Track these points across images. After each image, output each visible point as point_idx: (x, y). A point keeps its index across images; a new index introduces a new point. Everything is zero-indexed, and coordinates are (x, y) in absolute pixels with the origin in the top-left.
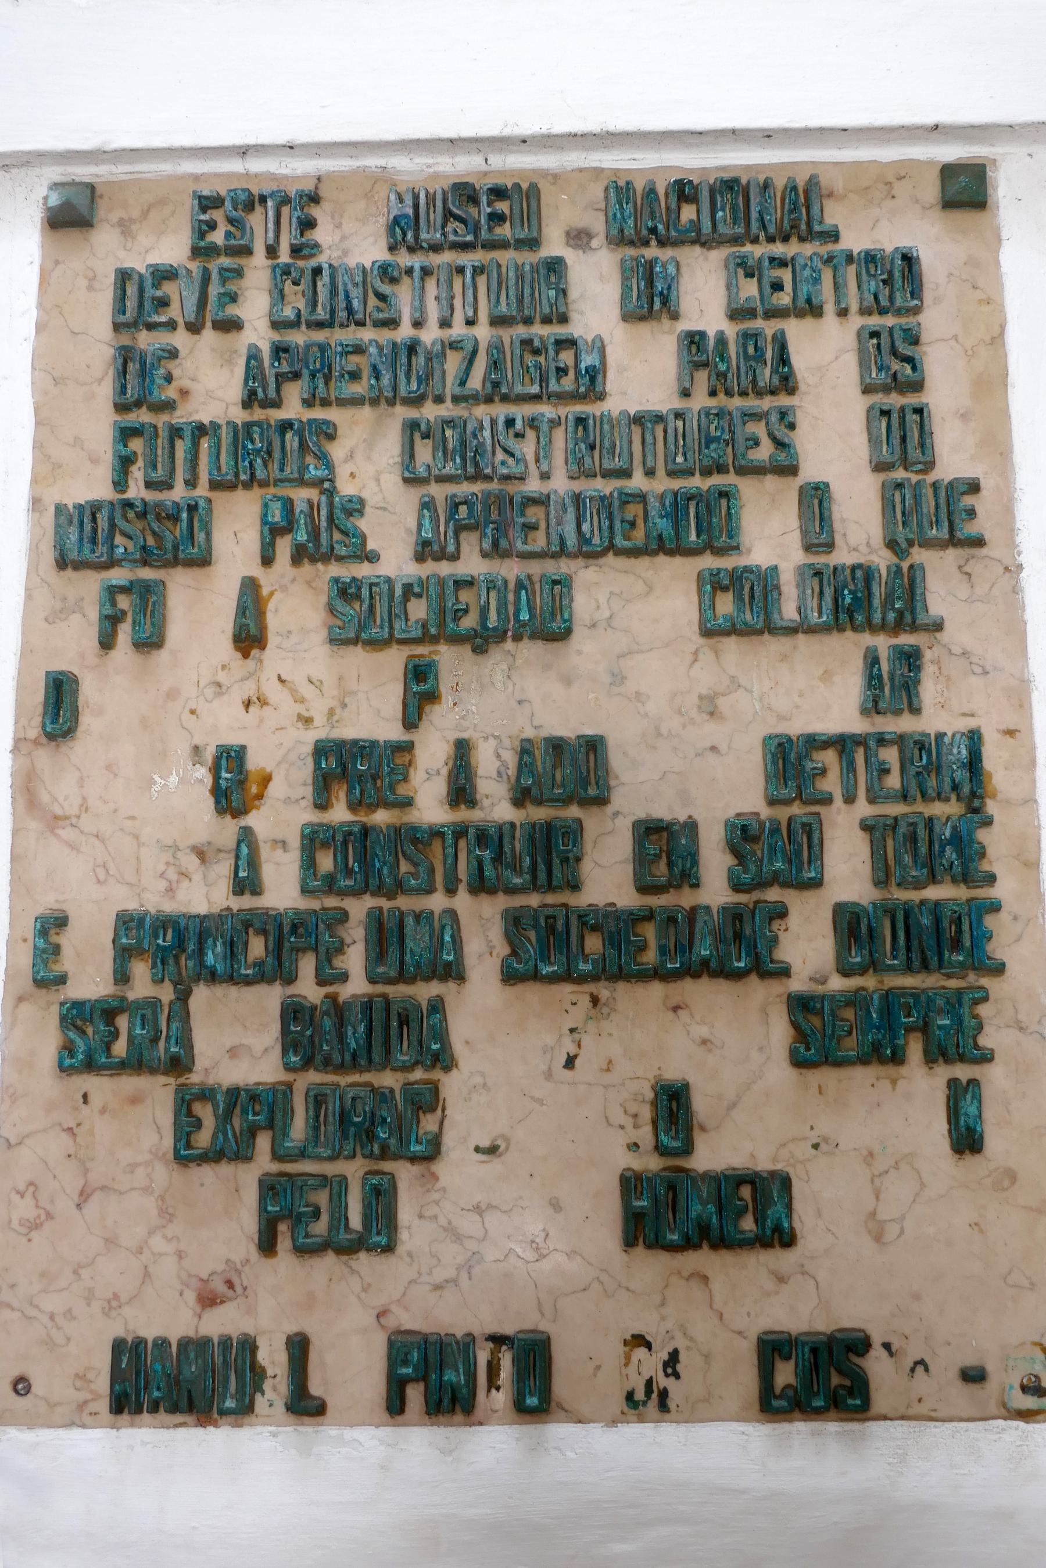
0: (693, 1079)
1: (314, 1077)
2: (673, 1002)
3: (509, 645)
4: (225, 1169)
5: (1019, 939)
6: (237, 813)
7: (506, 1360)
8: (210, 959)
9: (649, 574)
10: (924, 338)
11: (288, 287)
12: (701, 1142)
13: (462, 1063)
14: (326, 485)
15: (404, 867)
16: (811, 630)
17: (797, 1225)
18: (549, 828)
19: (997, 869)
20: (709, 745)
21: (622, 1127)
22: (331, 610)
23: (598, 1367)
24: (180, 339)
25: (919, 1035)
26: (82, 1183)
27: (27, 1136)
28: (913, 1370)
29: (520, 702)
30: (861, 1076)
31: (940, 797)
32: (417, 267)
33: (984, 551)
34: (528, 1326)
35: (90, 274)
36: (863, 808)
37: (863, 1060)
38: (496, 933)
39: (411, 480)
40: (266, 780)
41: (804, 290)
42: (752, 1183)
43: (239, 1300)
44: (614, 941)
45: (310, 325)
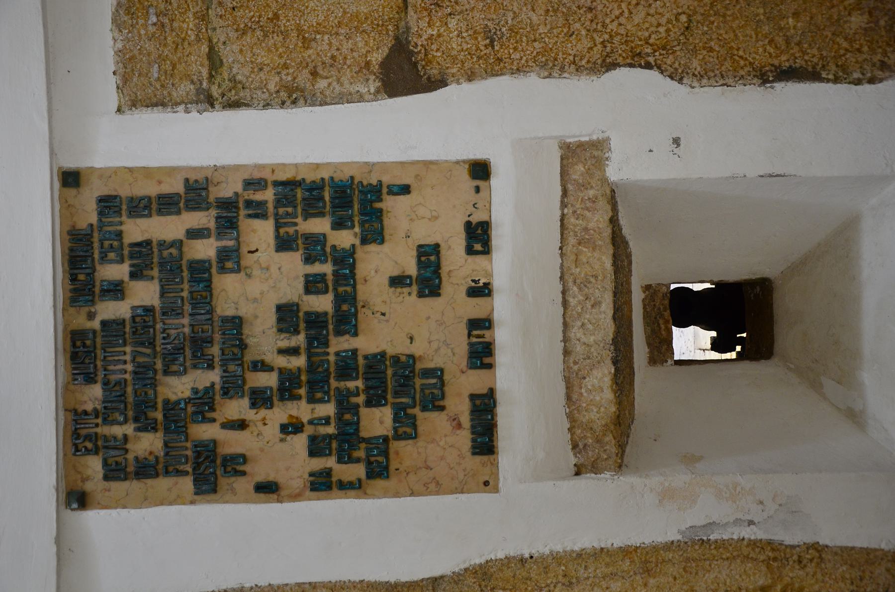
0: (388, 276)
1: (389, 397)
2: (364, 282)
3: (244, 337)
4: (418, 423)
5: (342, 171)
6: (303, 425)
7: (475, 332)
8: (352, 431)
9: (218, 290)
10: (130, 195)
11: (110, 419)
12: (407, 273)
13: (384, 349)
14: (187, 401)
15: (320, 369)
16: (238, 235)
17: (433, 243)
18: (306, 322)
19: (319, 177)
20: (278, 270)
21: (403, 297)
22: (231, 398)
23: (477, 304)
24: (130, 456)
25: (373, 204)
26: (424, 469)
27: (409, 487)
28: (476, 208)
29: (264, 333)
30: (386, 222)
31: (295, 196)
32: (104, 373)
33: (209, 177)
34: (465, 326)
35: (104, 491)
36: (299, 220)
37: (381, 222)
38: (342, 339)
39: (185, 372)
40: (291, 416)
41: (113, 236)
42: (420, 256)
43: (459, 416)
44: (345, 301)
45: (126, 410)
